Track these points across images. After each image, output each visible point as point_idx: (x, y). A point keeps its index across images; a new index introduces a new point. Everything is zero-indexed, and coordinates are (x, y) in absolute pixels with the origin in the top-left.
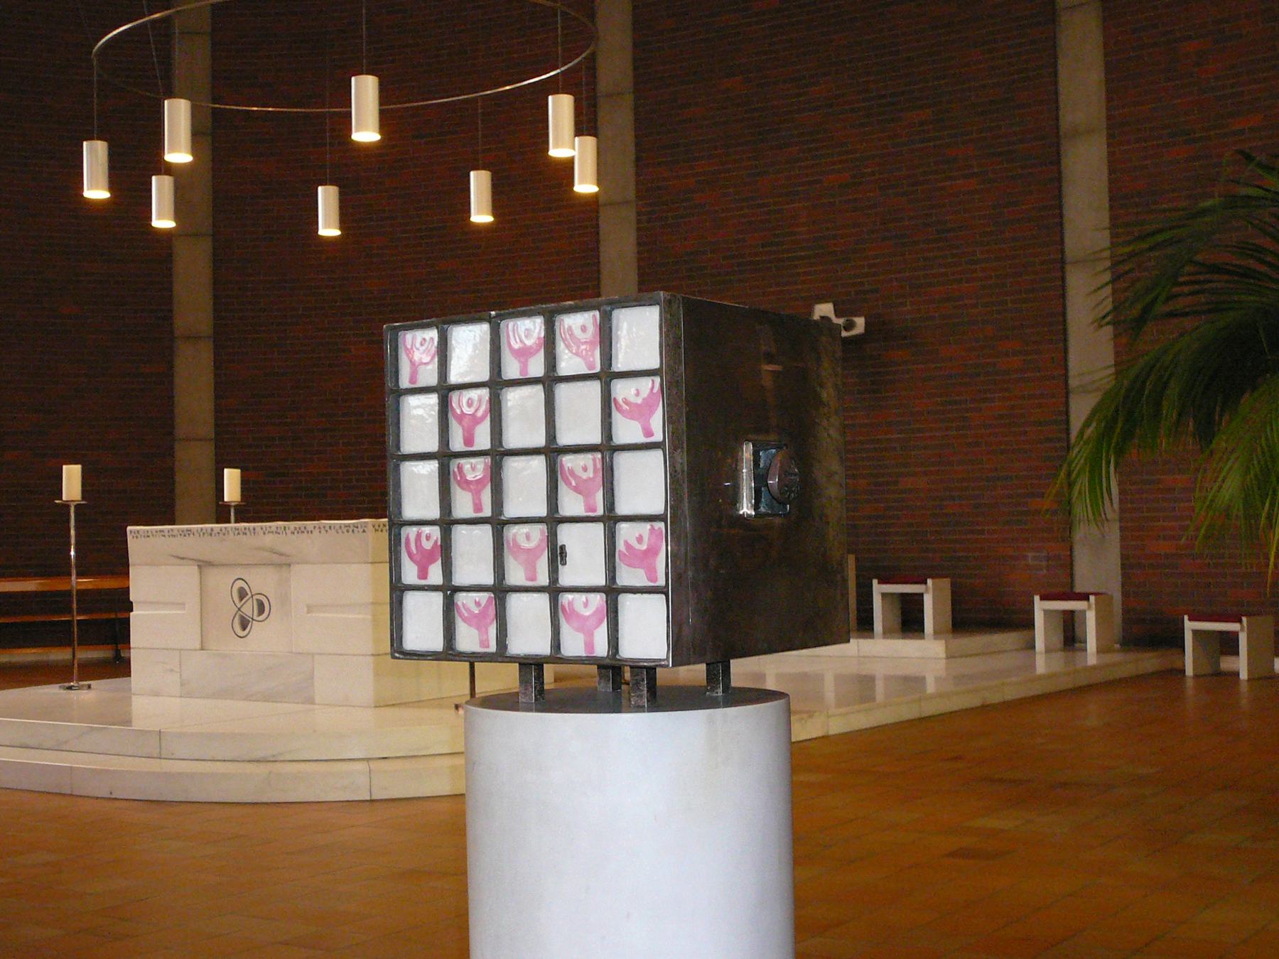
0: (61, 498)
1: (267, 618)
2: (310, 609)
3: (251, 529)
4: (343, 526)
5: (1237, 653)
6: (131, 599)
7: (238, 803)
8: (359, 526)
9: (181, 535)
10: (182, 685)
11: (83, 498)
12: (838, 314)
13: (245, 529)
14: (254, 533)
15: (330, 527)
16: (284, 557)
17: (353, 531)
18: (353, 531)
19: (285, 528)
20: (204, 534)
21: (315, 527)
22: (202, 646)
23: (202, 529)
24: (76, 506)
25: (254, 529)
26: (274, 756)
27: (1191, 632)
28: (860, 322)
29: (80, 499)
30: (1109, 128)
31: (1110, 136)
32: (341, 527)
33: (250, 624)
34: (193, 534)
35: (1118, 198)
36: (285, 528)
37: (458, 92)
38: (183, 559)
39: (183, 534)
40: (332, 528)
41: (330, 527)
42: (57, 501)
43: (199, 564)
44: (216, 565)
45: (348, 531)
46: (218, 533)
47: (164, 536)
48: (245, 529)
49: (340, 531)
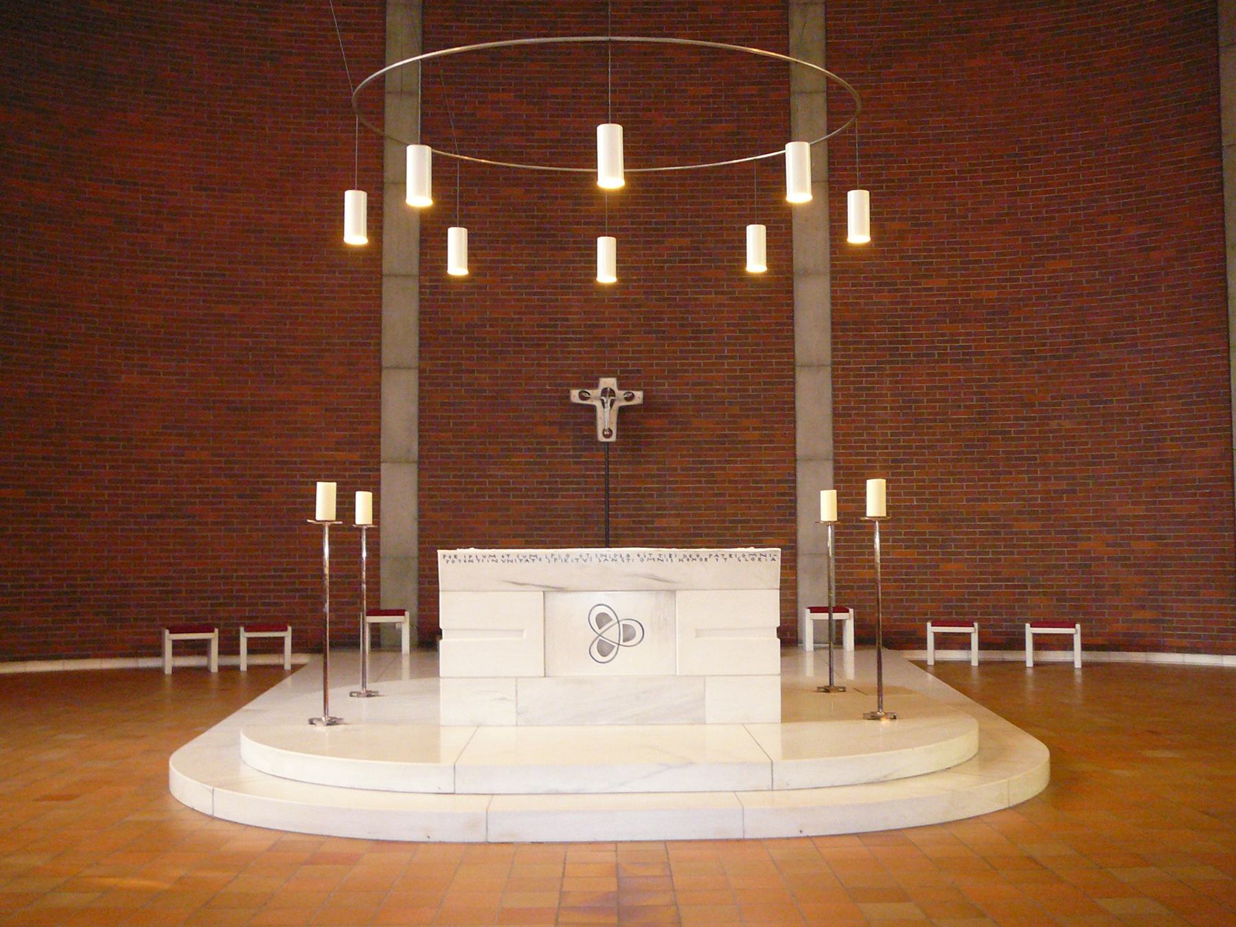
0: (313, 517)
1: (640, 642)
2: (698, 633)
3: (624, 556)
4: (747, 555)
5: (1024, 649)
6: (441, 626)
7: (236, 823)
8: (768, 555)
9: (521, 560)
10: (518, 714)
11: (338, 517)
12: (621, 387)
13: (615, 555)
14: (628, 560)
15: (730, 556)
16: (669, 584)
17: (759, 559)
18: (759, 559)
19: (670, 556)
20: (555, 559)
21: (710, 555)
22: (545, 673)
23: (553, 555)
24: (331, 528)
25: (628, 556)
26: (885, 776)
27: (933, 634)
28: (639, 395)
29: (334, 518)
30: (832, 272)
31: (833, 278)
32: (744, 556)
33: (615, 649)
34: (540, 560)
35: (838, 324)
36: (670, 556)
37: (771, 149)
38: (522, 584)
39: (524, 560)
40: (673, 556)
41: (730, 556)
42: (309, 521)
43: (544, 590)
44: (570, 591)
45: (753, 559)
46: (577, 559)
47: (497, 561)
48: (615, 555)
49: (742, 559)
